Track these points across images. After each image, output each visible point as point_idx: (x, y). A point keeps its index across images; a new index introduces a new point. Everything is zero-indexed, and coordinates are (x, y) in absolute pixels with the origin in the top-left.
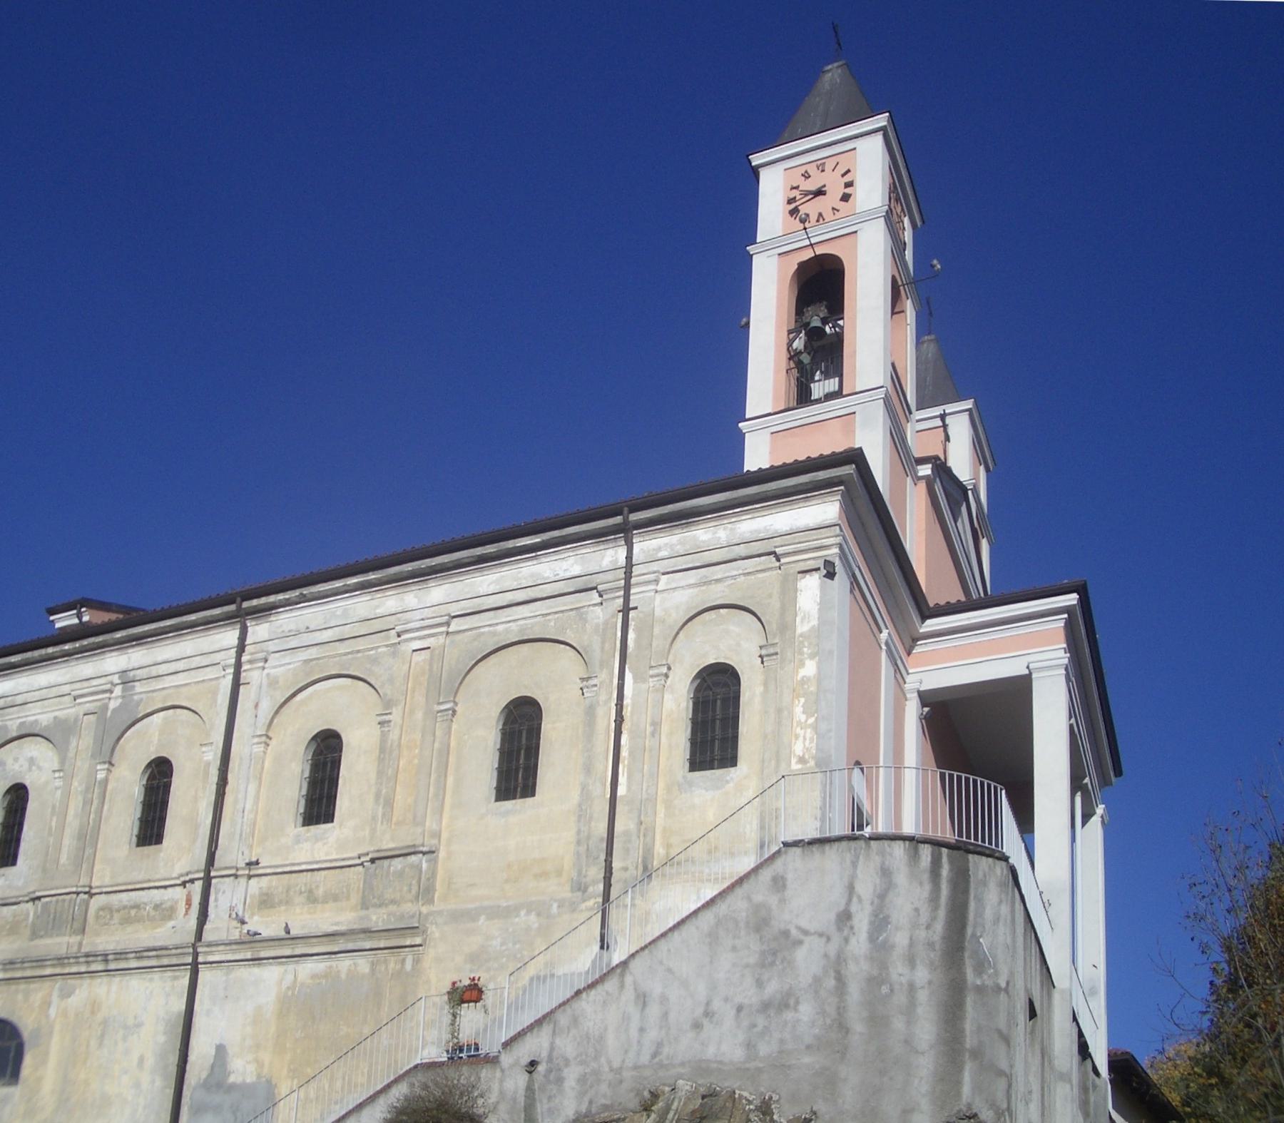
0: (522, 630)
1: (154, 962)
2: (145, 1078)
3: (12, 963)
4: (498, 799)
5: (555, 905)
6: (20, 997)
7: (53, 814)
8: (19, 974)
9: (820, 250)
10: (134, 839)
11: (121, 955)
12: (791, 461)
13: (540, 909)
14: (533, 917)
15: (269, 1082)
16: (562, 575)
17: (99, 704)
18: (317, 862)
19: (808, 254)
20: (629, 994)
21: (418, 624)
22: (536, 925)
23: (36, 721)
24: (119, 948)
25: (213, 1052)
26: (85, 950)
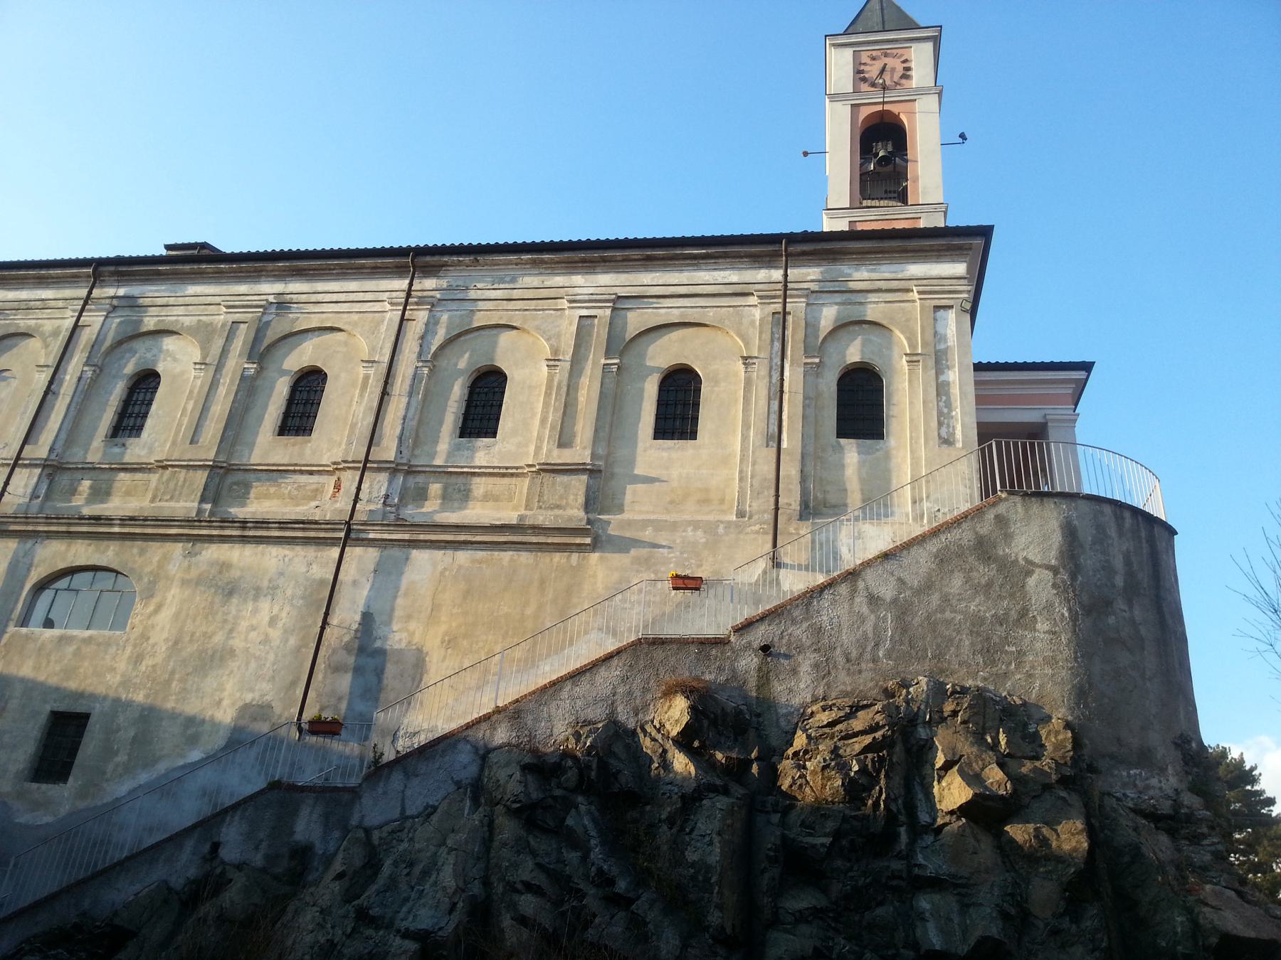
0: (682, 315)
1: (300, 534)
2: (275, 634)
3: (132, 519)
4: (693, 436)
5: (722, 526)
6: (135, 551)
7: (188, 399)
8: (138, 530)
9: (887, 107)
10: (458, 432)
11: (262, 524)
12: (799, 231)
13: (710, 528)
14: (700, 533)
15: (419, 650)
16: (720, 281)
17: (250, 315)
18: (494, 468)
19: (879, 108)
20: (860, 600)
21: (586, 297)
22: (703, 540)
23: (177, 321)
24: (259, 517)
25: (358, 618)
26: (48, 512)
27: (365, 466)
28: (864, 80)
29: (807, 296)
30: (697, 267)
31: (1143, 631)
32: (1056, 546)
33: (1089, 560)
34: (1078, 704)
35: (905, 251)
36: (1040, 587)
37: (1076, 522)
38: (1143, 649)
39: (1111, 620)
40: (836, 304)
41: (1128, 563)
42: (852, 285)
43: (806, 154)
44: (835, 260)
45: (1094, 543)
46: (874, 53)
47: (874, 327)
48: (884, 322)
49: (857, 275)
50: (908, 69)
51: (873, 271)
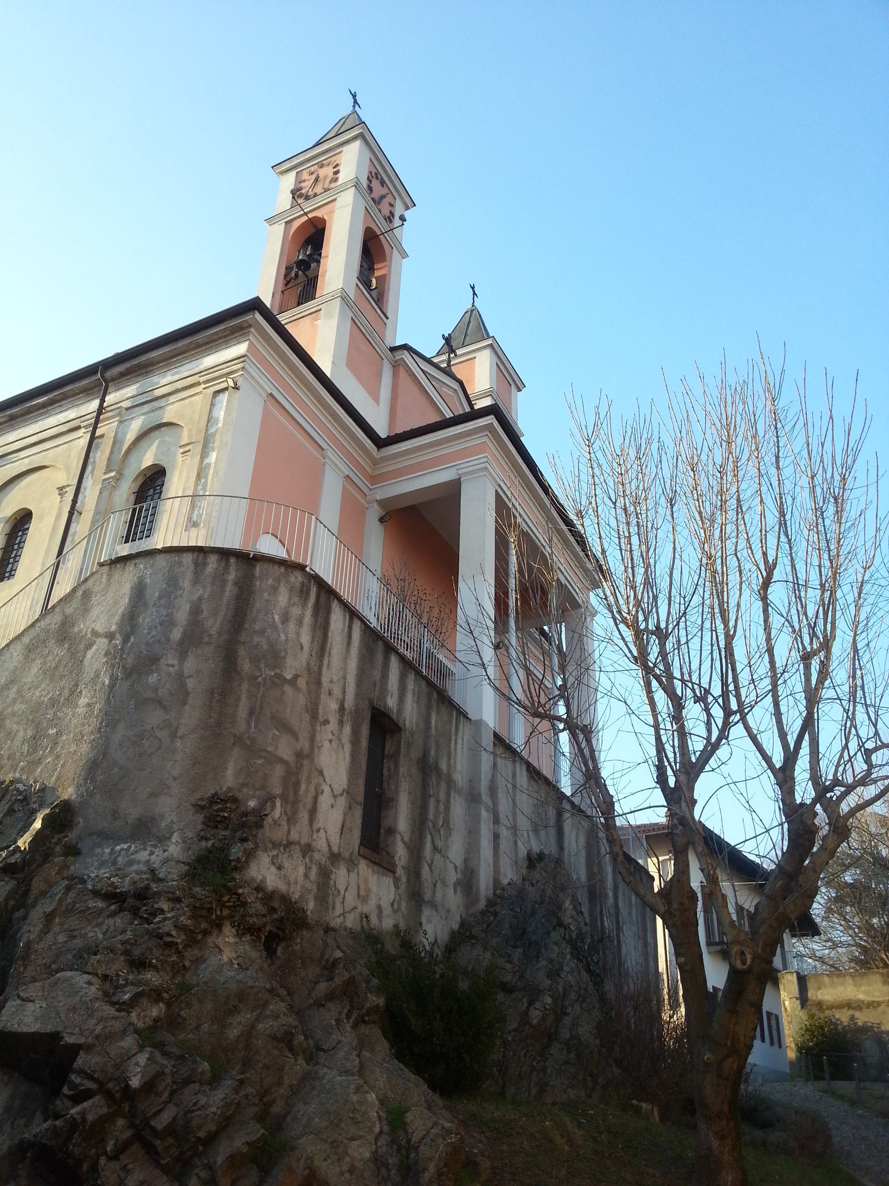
9: (310, 216)
19: (305, 218)
27: (687, 642)
28: (300, 196)
29: (120, 414)
30: (47, 414)
31: (191, 684)
32: (120, 612)
33: (146, 620)
34: (85, 780)
35: (199, 346)
36: (95, 659)
37: (148, 581)
38: (185, 703)
39: (153, 679)
40: (142, 414)
41: (196, 611)
42: (158, 393)
43: (473, 288)
44: (147, 373)
45: (160, 598)
46: (312, 169)
47: (169, 428)
48: (175, 421)
49: (164, 381)
50: (337, 173)
51: (177, 373)
